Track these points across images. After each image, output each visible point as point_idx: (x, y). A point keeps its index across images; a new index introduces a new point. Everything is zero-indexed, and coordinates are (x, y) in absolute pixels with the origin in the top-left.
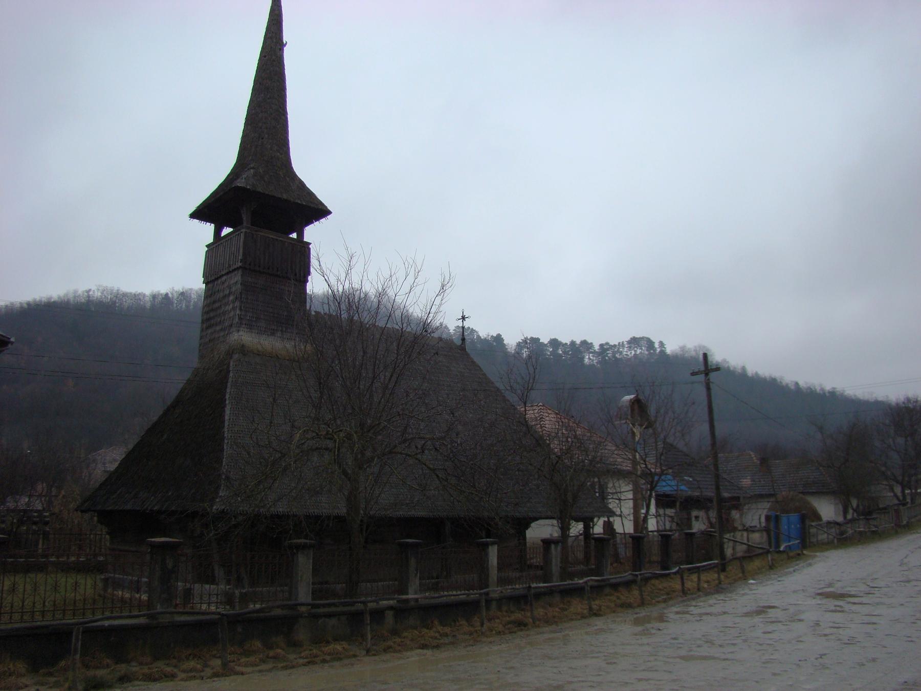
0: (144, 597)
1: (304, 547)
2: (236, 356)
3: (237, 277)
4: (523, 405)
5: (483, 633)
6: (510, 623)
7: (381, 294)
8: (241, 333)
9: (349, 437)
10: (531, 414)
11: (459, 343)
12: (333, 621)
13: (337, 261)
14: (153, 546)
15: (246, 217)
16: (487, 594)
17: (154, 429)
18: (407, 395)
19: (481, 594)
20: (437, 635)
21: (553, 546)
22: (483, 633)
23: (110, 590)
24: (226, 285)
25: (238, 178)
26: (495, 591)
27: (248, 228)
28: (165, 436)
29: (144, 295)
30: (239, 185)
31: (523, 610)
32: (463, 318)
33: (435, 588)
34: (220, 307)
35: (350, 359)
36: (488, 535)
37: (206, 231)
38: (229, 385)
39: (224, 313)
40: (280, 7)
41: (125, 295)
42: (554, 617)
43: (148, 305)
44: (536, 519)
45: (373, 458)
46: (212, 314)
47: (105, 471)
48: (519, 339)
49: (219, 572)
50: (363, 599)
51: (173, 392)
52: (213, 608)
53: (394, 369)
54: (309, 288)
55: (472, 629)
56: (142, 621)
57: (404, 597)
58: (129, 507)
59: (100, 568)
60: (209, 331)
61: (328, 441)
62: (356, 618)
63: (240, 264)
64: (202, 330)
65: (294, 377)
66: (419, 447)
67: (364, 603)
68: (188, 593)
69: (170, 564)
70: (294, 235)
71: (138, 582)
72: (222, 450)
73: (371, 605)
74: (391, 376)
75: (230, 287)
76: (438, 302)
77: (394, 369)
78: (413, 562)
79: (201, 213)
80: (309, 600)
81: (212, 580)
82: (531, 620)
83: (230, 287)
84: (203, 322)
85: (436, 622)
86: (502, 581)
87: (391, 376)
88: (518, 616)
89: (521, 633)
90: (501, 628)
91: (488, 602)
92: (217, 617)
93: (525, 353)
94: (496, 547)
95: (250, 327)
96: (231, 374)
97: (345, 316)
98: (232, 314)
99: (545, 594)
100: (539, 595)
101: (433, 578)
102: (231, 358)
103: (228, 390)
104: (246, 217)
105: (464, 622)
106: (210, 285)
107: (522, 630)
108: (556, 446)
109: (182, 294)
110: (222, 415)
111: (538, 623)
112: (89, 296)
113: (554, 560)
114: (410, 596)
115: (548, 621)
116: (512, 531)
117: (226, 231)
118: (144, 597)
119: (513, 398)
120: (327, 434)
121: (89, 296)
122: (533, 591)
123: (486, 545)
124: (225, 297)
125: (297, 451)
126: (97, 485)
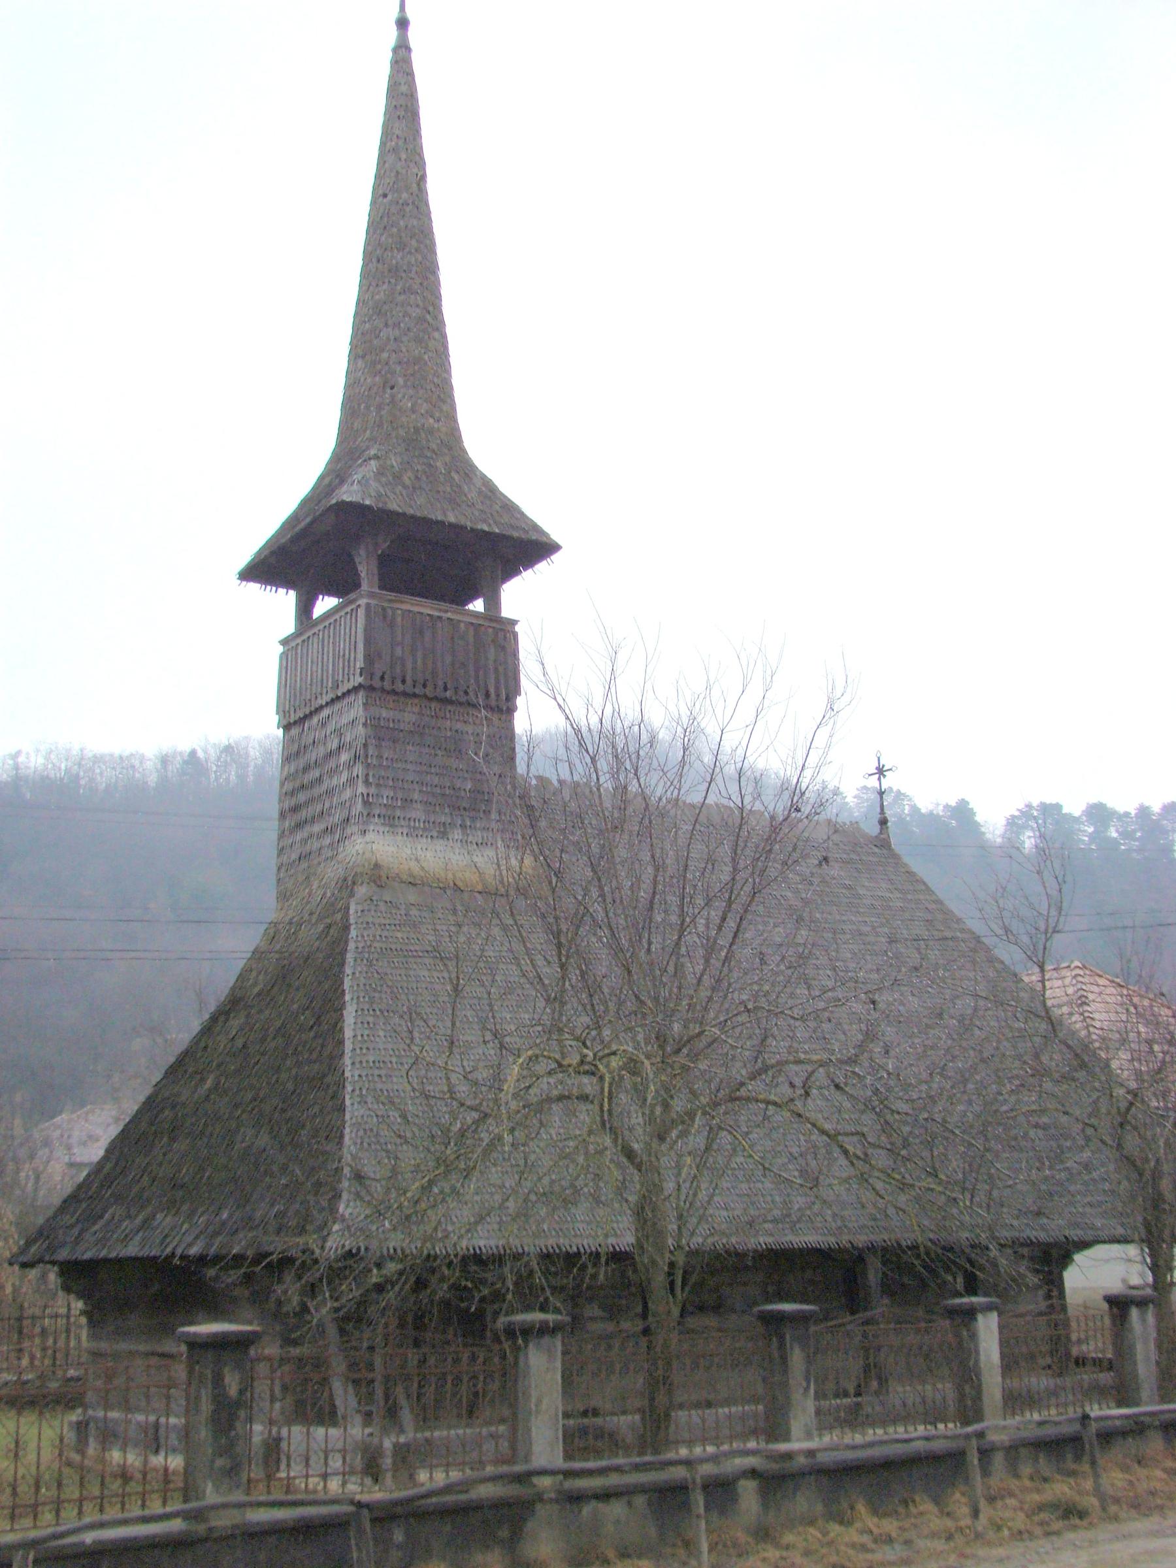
0: (176, 1462)
1: (544, 1330)
2: (362, 891)
3: (355, 709)
4: (1037, 970)
5: (978, 1536)
6: (1041, 1508)
7: (690, 733)
8: (371, 836)
9: (632, 1066)
10: (1058, 990)
11: (873, 829)
12: (616, 1509)
13: (582, 659)
14: (197, 1345)
15: (366, 569)
16: (980, 1435)
17: (182, 1067)
18: (763, 962)
19: (967, 1437)
20: (865, 1539)
21: (1134, 1312)
22: (978, 1536)
23: (92, 1449)
24: (331, 727)
25: (342, 481)
26: (1000, 1426)
27: (371, 595)
28: (209, 1083)
29: (142, 759)
30: (347, 498)
31: (1073, 1474)
32: (881, 771)
33: (853, 1418)
34: (319, 780)
35: (626, 892)
36: (972, 1288)
37: (281, 604)
38: (350, 957)
39: (330, 793)
40: (410, 74)
41: (97, 759)
42: (1153, 1493)
43: (153, 779)
44: (1084, 1245)
45: (691, 1115)
46: (302, 797)
47: (71, 1165)
48: (1013, 807)
49: (343, 1396)
50: (683, 1452)
51: (221, 981)
52: (334, 1485)
53: (730, 902)
54: (521, 723)
55: (950, 1523)
56: (176, 1525)
57: (783, 1447)
58: (132, 1250)
59: (67, 1400)
60: (299, 836)
61: (586, 1080)
62: (670, 1499)
63: (359, 680)
64: (281, 836)
65: (496, 931)
66: (798, 1082)
67: (688, 1463)
68: (273, 1451)
69: (232, 1383)
70: (478, 605)
71: (157, 1426)
72: (341, 1109)
73: (707, 1469)
74: (724, 919)
75: (339, 733)
76: (821, 740)
77: (730, 902)
78: (797, 1357)
79: (267, 568)
80: (559, 1462)
81: (328, 1416)
82: (1095, 1501)
83: (339, 733)
84: (283, 815)
85: (861, 1507)
86: (1014, 1401)
87: (724, 919)
88: (1061, 1489)
89: (1071, 1536)
90: (1020, 1521)
91: (985, 1453)
92: (351, 1509)
93: (1028, 841)
94: (994, 1317)
95: (390, 821)
96: (353, 933)
97: (607, 784)
98: (348, 793)
99: (1124, 1434)
100: (1107, 1437)
101: (846, 1394)
102: (352, 895)
103: (348, 970)
104: (366, 569)
105: (928, 1506)
106: (295, 731)
107: (1075, 1528)
108: (1120, 1063)
109: (228, 749)
110: (336, 1026)
111: (1113, 1509)
112: (17, 767)
113: (1139, 1347)
114: (794, 1446)
115: (1139, 1506)
116: (1033, 1279)
117: (325, 604)
118: (176, 1462)
119: (1008, 954)
120: (582, 1062)
121: (17, 767)
122: (1094, 1427)
123: (970, 1313)
124: (330, 755)
125: (514, 1105)
126: (57, 1201)
